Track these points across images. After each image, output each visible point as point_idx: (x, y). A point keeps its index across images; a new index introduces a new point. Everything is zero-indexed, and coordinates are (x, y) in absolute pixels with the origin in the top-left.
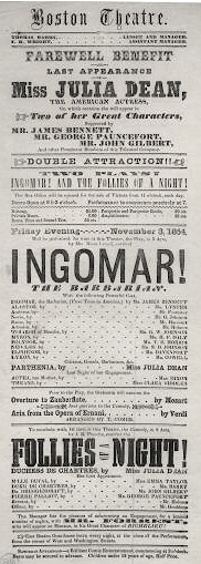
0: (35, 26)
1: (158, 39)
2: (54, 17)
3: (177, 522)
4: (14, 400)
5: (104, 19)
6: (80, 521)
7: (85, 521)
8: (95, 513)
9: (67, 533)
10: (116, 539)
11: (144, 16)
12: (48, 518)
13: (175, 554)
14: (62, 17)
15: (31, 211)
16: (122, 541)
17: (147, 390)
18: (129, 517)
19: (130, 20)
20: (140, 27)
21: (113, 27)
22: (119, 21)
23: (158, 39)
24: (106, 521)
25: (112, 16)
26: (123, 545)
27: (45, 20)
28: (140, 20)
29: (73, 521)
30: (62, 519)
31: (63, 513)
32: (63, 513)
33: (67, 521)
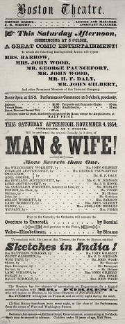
0: (20, 15)
1: (98, 23)
2: (32, 9)
3: (111, 290)
4: (6, 222)
5: (64, 10)
6: (48, 290)
7: (52, 290)
8: (58, 285)
9: (40, 301)
10: (72, 306)
11: (91, 9)
12: (28, 288)
13: (109, 316)
14: (37, 9)
15: (18, 104)
16: (75, 307)
17: (95, 215)
18: (80, 287)
19: (80, 11)
20: (87, 16)
21: (70, 15)
22: (73, 13)
23: (98, 23)
24: (65, 290)
25: (69, 9)
26: (76, 310)
27: (27, 11)
28: (87, 11)
29: (44, 290)
30: (37, 289)
31: (38, 284)
32: (38, 284)
33: (41, 290)
